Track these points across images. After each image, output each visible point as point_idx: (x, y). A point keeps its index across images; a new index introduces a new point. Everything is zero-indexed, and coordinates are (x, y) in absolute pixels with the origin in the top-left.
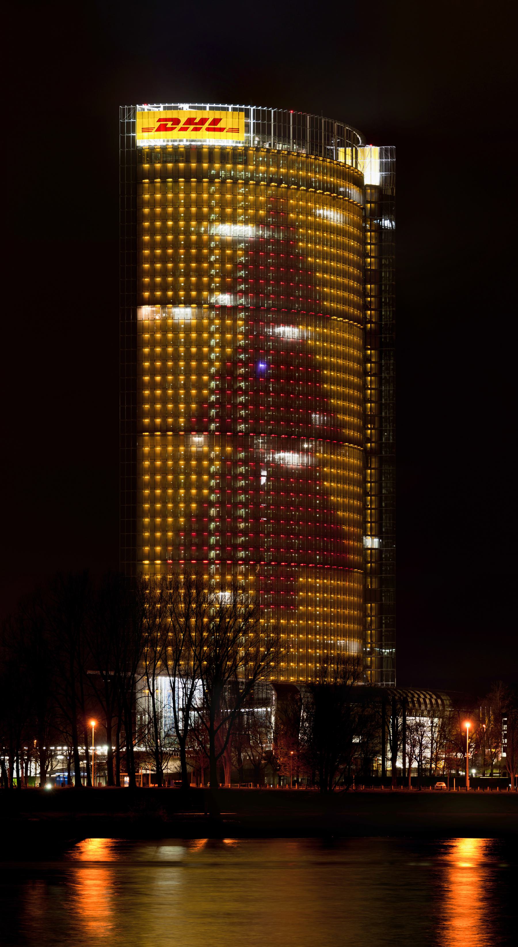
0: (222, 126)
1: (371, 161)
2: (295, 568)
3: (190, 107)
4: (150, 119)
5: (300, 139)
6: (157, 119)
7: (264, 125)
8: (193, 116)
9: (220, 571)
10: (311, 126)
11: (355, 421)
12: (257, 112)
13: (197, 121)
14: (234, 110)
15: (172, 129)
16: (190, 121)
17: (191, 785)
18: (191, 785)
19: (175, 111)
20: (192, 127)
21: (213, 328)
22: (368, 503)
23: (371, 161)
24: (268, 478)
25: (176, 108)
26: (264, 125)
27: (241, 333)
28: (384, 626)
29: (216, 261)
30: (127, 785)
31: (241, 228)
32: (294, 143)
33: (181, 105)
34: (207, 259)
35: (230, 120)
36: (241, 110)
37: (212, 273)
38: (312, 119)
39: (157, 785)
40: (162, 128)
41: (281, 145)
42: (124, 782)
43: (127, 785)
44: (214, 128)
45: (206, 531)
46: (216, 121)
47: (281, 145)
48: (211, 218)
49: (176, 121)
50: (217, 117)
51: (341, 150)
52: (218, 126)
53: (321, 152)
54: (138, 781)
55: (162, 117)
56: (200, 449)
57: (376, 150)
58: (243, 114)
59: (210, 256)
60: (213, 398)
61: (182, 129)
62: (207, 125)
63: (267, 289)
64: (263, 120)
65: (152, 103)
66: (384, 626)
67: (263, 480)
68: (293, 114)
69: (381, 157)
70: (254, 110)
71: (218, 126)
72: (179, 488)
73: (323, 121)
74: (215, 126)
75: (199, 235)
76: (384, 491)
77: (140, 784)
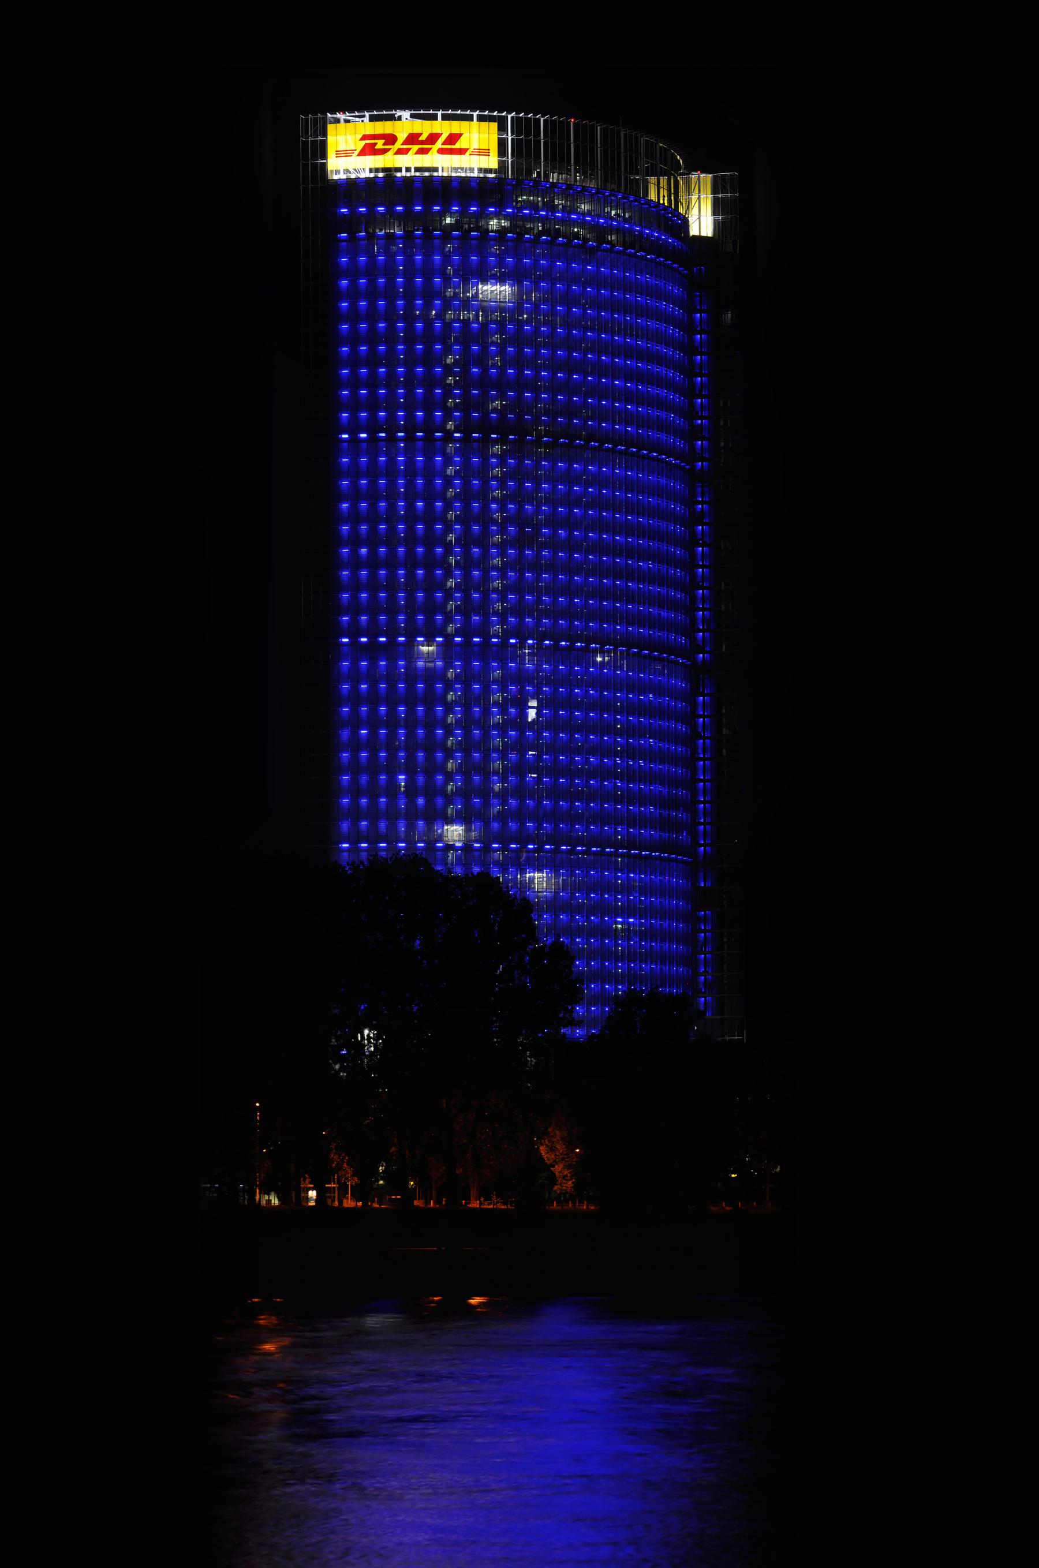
0: (463, 147)
1: (699, 198)
2: (583, 855)
3: (412, 116)
4: (349, 137)
5: (586, 163)
6: (360, 136)
7: (528, 142)
8: (417, 131)
9: (461, 340)
10: (604, 143)
11: (676, 485)
12: (516, 121)
13: (423, 138)
14: (481, 119)
15: (384, 152)
16: (413, 138)
17: (416, 1203)
18: (416, 1203)
19: (389, 123)
20: (415, 148)
21: (450, 470)
22: (700, 750)
23: (699, 198)
24: (539, 709)
25: (391, 118)
26: (528, 142)
27: (495, 546)
28: (726, 946)
29: (457, 703)
30: (312, 1203)
31: (494, 288)
32: (576, 171)
33: (399, 113)
34: (441, 609)
35: (475, 136)
36: (491, 119)
37: (448, 382)
38: (604, 131)
39: (361, 1203)
40: (369, 150)
41: (555, 175)
42: (308, 1199)
43: (312, 1203)
44: (451, 149)
45: (440, 568)
46: (453, 138)
47: (555, 175)
48: (448, 316)
49: (391, 139)
50: (456, 131)
51: (653, 180)
52: (457, 146)
53: (619, 185)
54: (330, 1197)
55: (368, 133)
56: (431, 665)
57: (707, 178)
58: (494, 125)
59: (446, 288)
60: (451, 787)
61: (400, 152)
62: (439, 144)
63: (536, 407)
64: (528, 134)
65: (351, 111)
66: (726, 946)
67: (532, 714)
68: (575, 124)
69: (714, 213)
70: (512, 118)
71: (457, 146)
72: (397, 726)
73: (622, 134)
74: (452, 145)
75: (429, 323)
76: (725, 731)
77: (333, 1201)
